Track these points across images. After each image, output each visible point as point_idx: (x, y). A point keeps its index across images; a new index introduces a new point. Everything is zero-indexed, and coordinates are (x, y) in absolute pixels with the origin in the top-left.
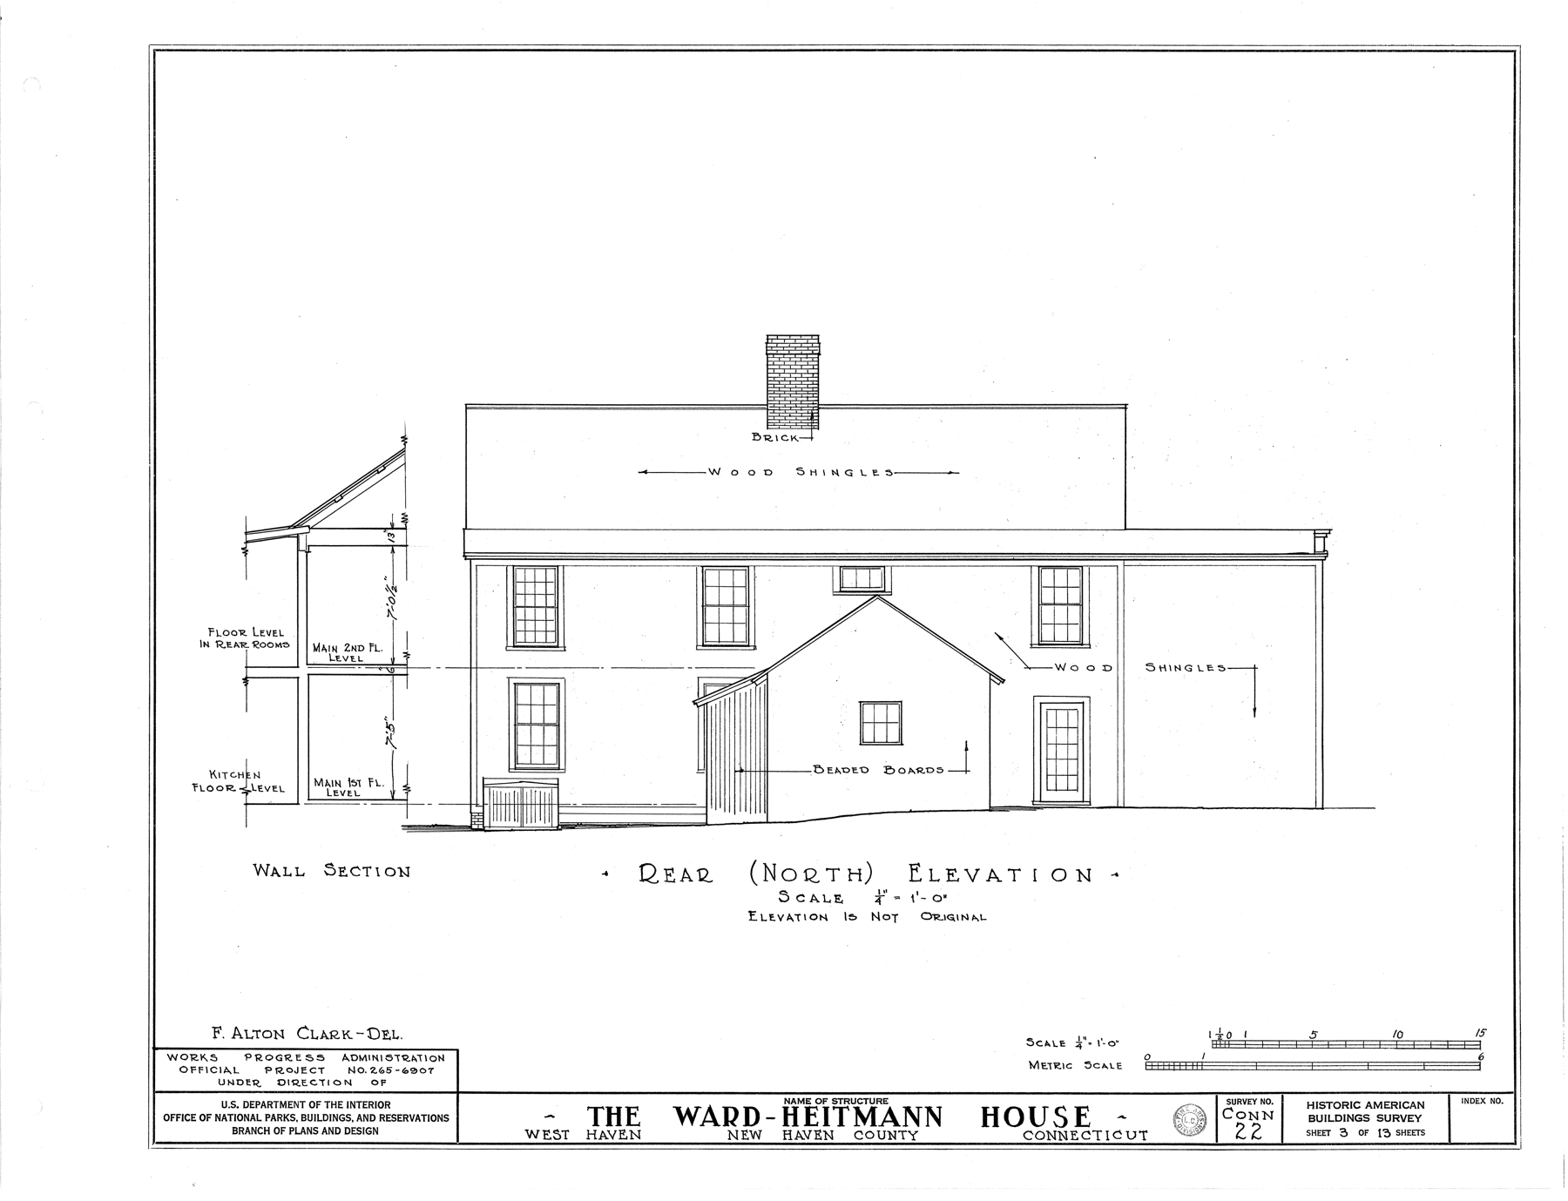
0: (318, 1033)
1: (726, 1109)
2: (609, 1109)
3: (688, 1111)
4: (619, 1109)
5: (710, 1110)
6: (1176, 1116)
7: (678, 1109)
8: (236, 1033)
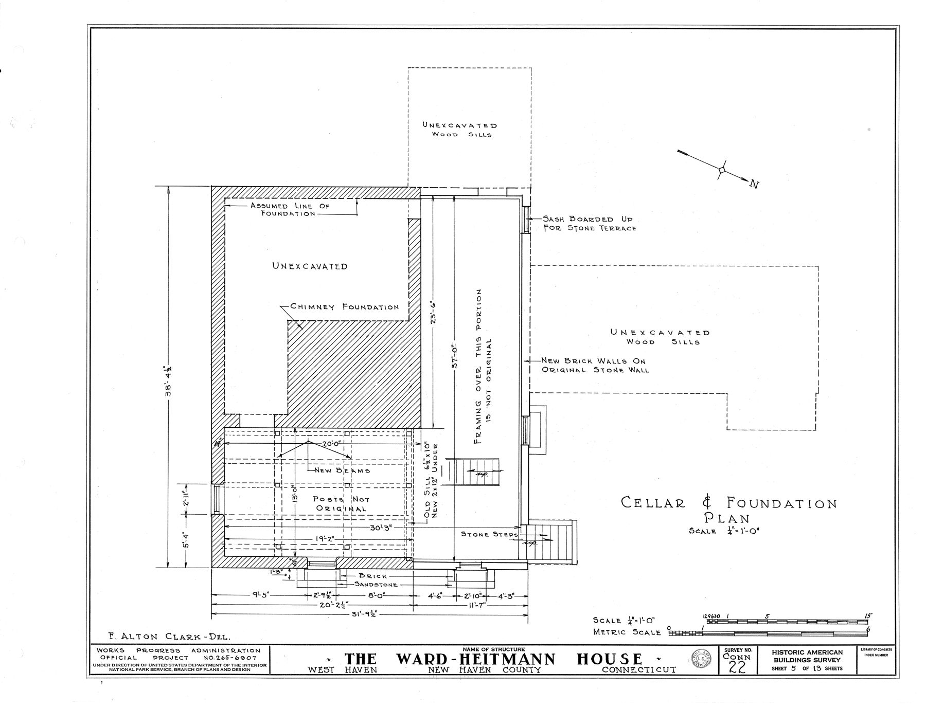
0: (178, 637)
1: (427, 655)
3: (405, 657)
6: (693, 657)
7: (399, 655)
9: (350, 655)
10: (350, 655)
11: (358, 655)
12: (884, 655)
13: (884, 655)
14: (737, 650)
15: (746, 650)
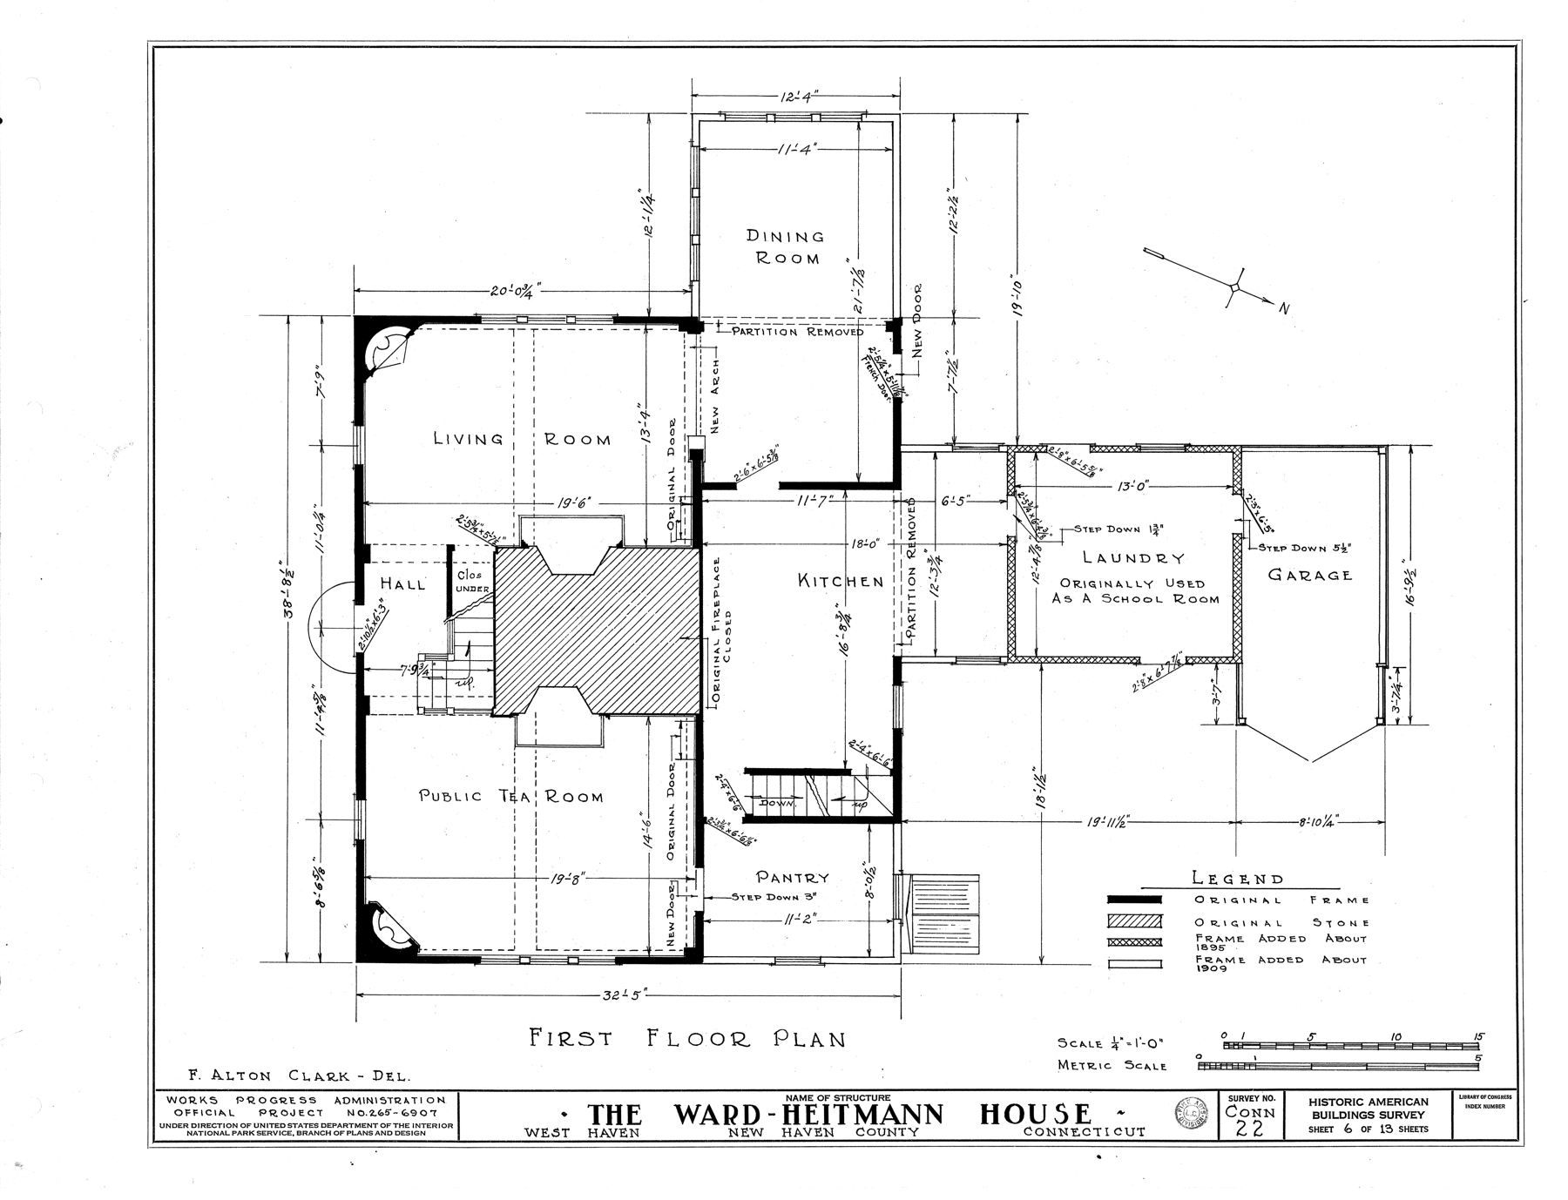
1: (726, 1107)
2: (609, 1107)
3: (689, 1110)
4: (619, 1107)
5: (709, 1108)
8: (216, 1075)
9: (596, 1108)
10: (596, 1108)
11: (609, 1107)
12: (1498, 1106)
13: (1498, 1106)
14: (1250, 1099)
15: (1265, 1098)
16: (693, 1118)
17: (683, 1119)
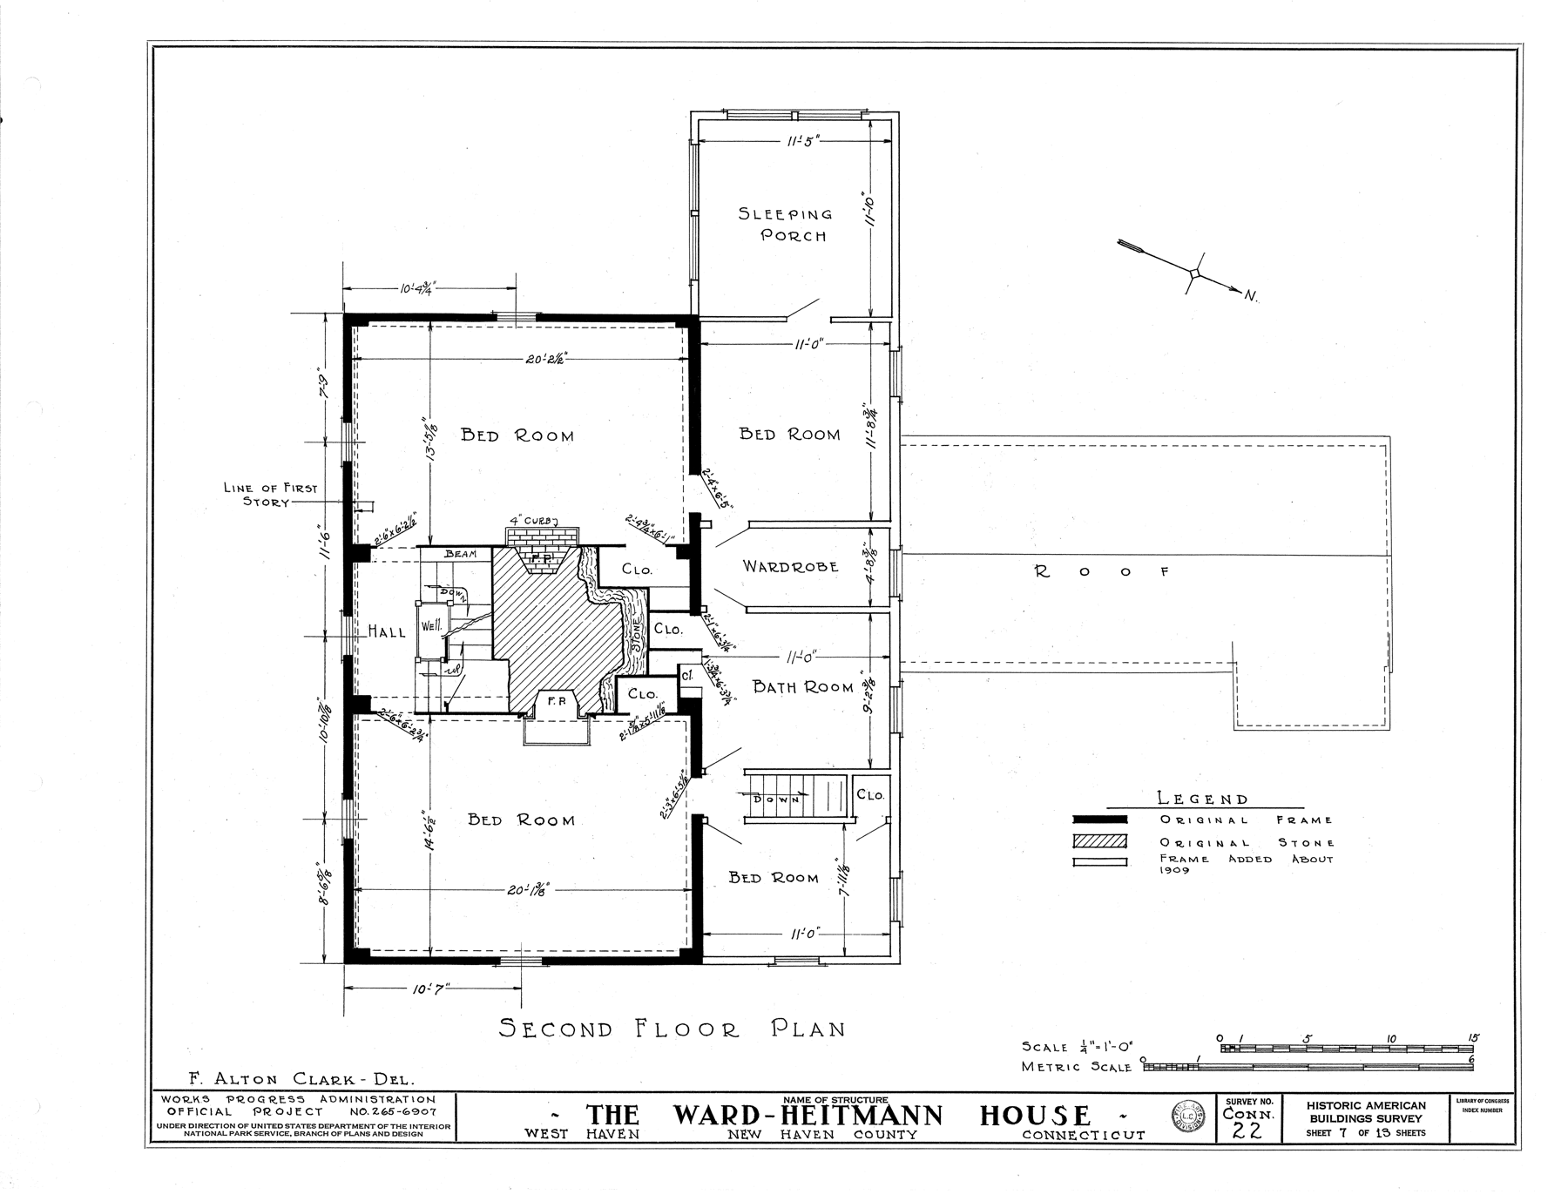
0: (317, 1079)
1: (725, 1108)
2: (609, 1107)
3: (687, 1110)
5: (708, 1111)
11: (609, 1107)
12: (1495, 1110)
13: (1495, 1110)
16: (691, 1118)
17: (681, 1118)
